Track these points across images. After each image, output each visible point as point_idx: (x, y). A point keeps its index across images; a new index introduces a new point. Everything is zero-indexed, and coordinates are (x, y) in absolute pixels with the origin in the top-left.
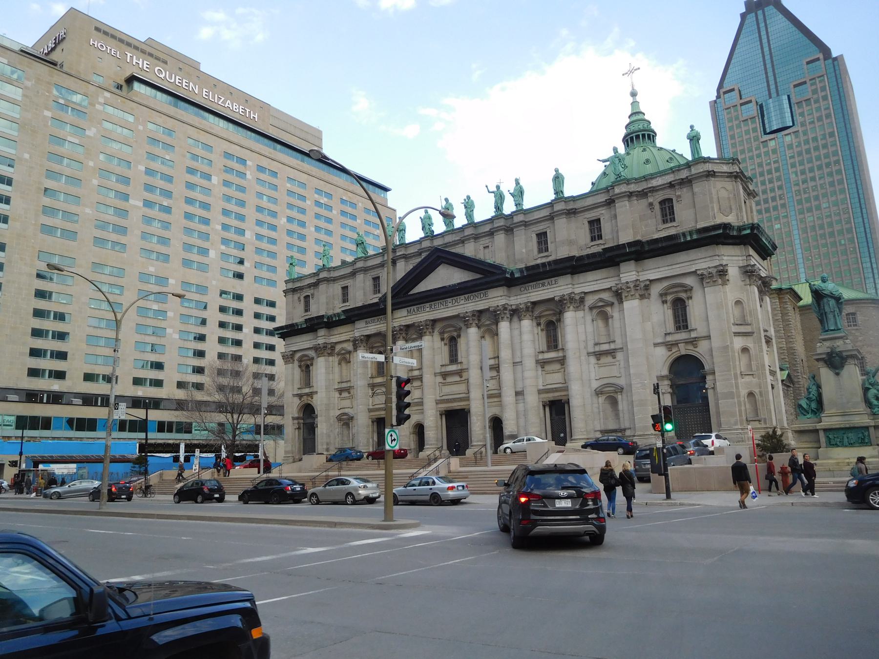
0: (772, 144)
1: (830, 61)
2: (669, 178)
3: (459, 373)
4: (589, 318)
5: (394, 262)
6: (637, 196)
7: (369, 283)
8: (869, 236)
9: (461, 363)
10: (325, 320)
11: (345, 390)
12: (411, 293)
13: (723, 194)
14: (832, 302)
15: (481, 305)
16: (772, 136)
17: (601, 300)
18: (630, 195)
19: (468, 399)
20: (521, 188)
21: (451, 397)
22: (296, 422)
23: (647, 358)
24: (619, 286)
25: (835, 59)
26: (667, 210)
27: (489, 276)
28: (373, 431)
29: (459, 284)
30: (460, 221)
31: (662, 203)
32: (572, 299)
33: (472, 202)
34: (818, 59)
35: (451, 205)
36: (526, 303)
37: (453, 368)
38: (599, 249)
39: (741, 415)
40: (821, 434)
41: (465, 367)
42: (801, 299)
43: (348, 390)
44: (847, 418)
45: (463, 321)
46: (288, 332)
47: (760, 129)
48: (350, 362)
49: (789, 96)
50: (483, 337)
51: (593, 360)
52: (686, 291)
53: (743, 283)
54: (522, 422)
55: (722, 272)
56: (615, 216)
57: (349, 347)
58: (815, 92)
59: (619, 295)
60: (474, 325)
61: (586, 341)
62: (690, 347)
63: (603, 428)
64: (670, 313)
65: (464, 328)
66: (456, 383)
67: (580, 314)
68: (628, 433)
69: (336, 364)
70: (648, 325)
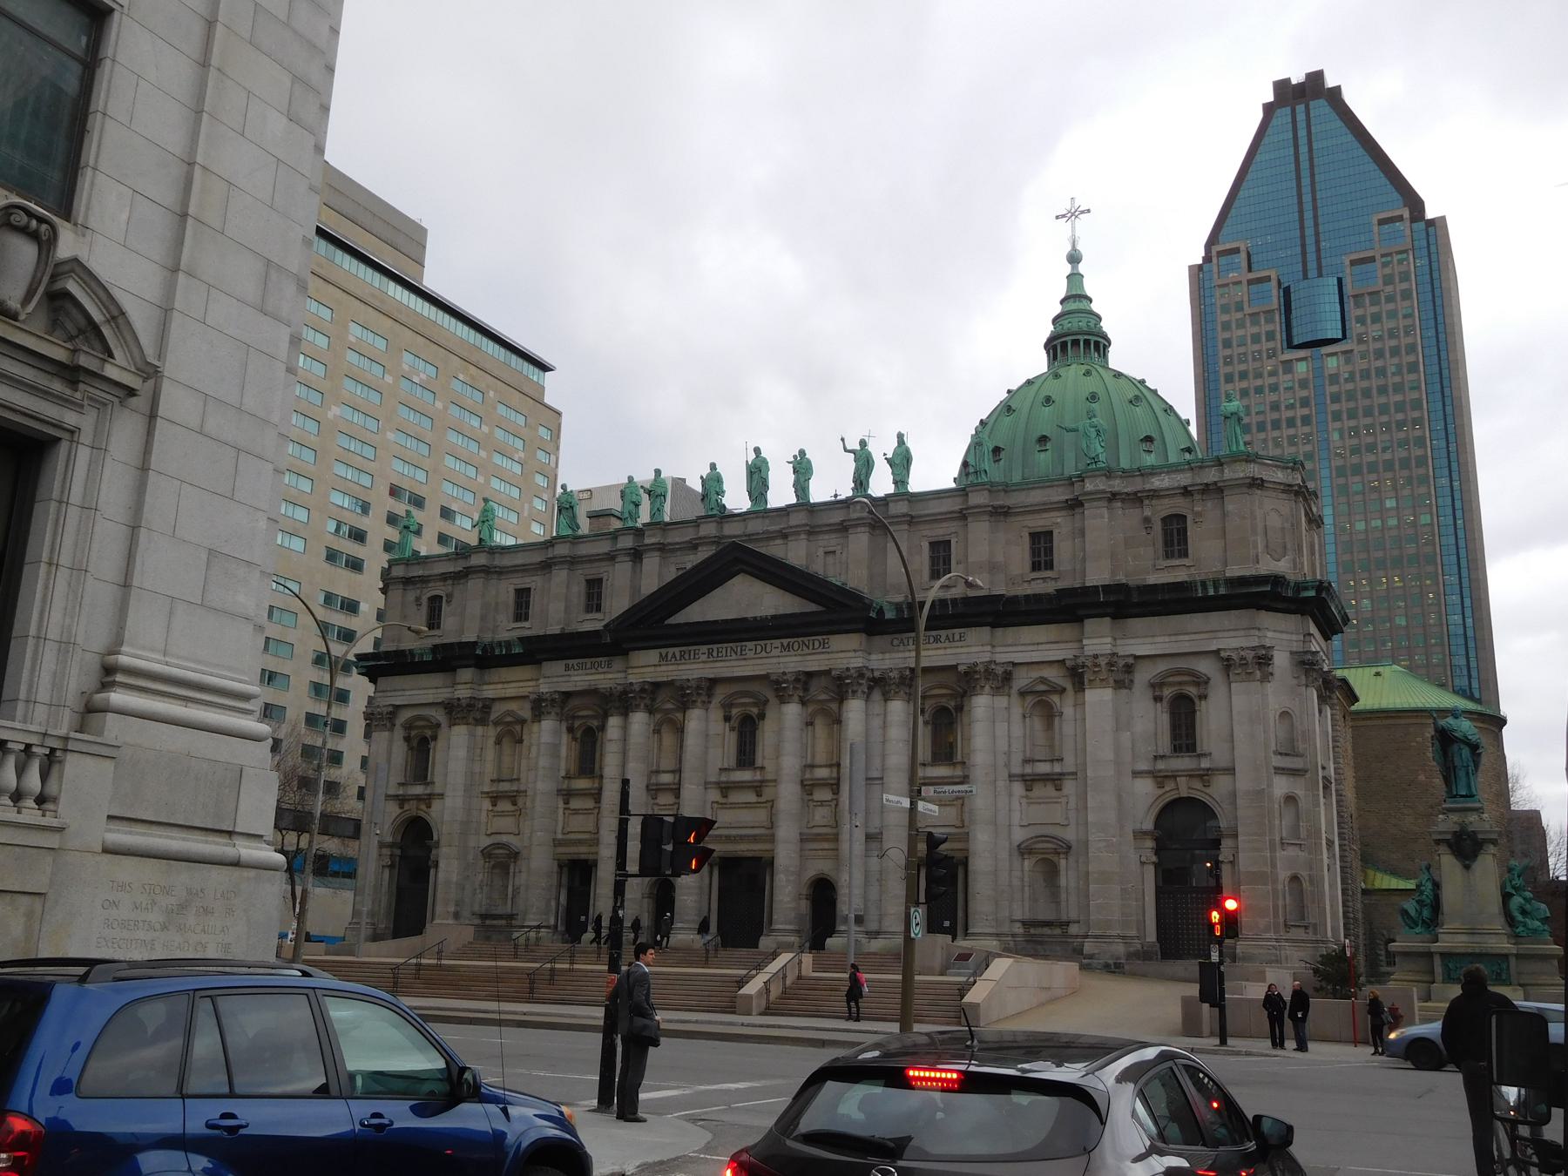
0: (1301, 368)
1: (1422, 225)
2: (1184, 479)
3: (758, 787)
4: (1017, 711)
5: (636, 555)
6: (1123, 501)
7: (579, 589)
8: (1464, 573)
9: (762, 768)
10: (479, 652)
11: (507, 795)
12: (672, 621)
13: (1275, 521)
14: (1466, 752)
15: (814, 663)
16: (1302, 353)
17: (1043, 680)
18: (1114, 496)
19: (772, 839)
20: (908, 450)
21: (734, 832)
22: (386, 851)
23: (1119, 797)
24: (1079, 661)
25: (1432, 223)
26: (1175, 536)
27: (835, 610)
28: (560, 885)
29: (774, 617)
30: (781, 494)
31: (1166, 520)
32: (989, 673)
33: (809, 462)
34: (1401, 218)
35: (765, 461)
36: (901, 670)
37: (745, 776)
38: (1049, 588)
39: (1276, 915)
40: (1437, 961)
41: (769, 777)
42: (1357, 700)
43: (513, 798)
44: (1477, 938)
45: (779, 688)
46: (378, 666)
47: (1280, 336)
48: (521, 741)
49: (1340, 281)
50: (810, 724)
51: (1018, 788)
52: (1197, 684)
53: (1295, 682)
54: (874, 893)
55: (1263, 660)
56: (1082, 533)
57: (525, 711)
58: (1388, 280)
59: (1077, 675)
60: (796, 698)
61: (1008, 754)
62: (1198, 784)
63: (1027, 916)
64: (1165, 719)
65: (773, 700)
66: (748, 806)
67: (1002, 701)
68: (1073, 929)
69: (491, 741)
70: (1126, 737)
